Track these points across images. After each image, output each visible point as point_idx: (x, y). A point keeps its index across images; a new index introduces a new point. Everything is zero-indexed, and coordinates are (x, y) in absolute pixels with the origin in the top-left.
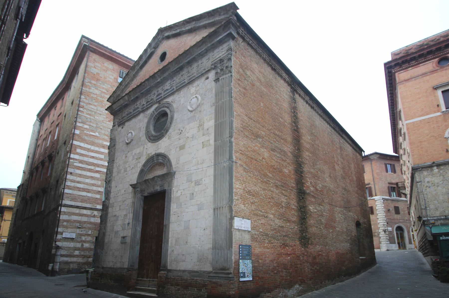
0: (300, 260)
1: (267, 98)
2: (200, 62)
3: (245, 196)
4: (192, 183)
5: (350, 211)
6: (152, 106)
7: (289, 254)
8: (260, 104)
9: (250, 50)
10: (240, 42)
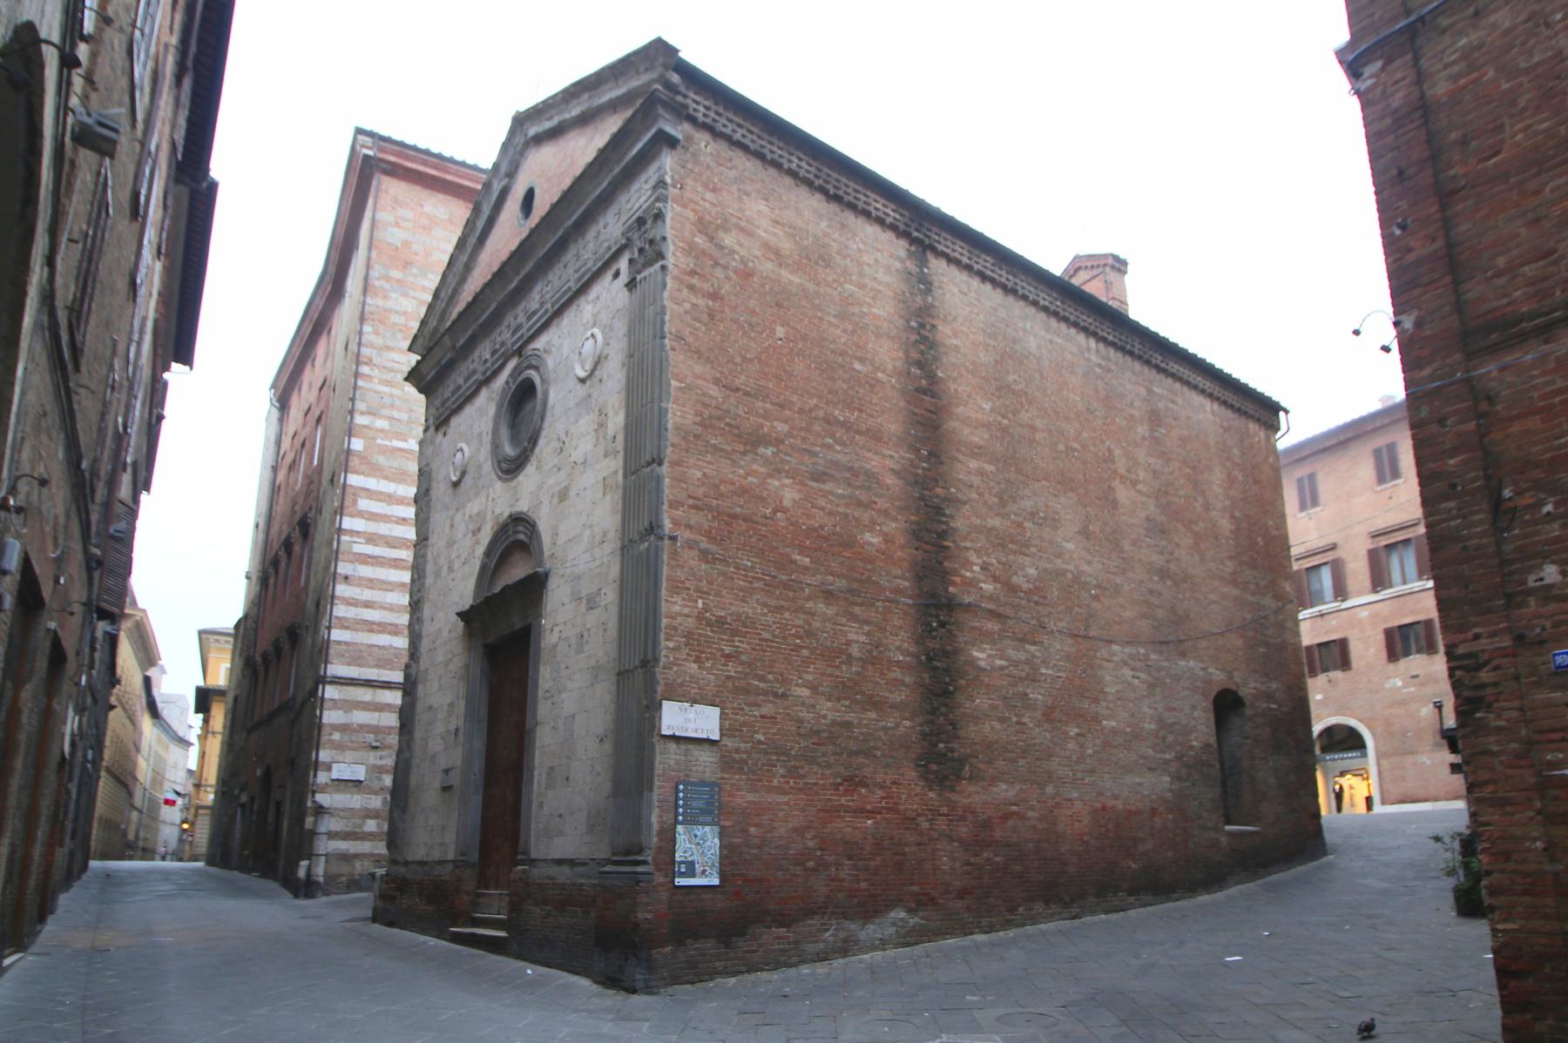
1: (803, 303)
2: (601, 224)
3: (705, 636)
5: (1183, 655)
8: (773, 331)
9: (739, 158)
10: (699, 144)
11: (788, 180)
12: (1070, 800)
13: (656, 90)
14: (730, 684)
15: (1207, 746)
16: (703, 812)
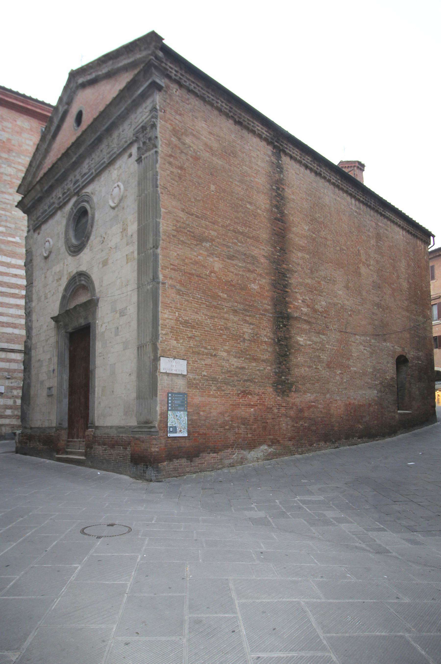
0: (272, 413)
1: (223, 174)
2: (121, 129)
3: (179, 328)
4: (116, 313)
5: (385, 341)
6: (69, 200)
7: (252, 405)
8: (209, 187)
10: (172, 90)
11: (216, 112)
12: (336, 400)
13: (150, 60)
14: (191, 350)
15: (392, 378)
16: (180, 405)
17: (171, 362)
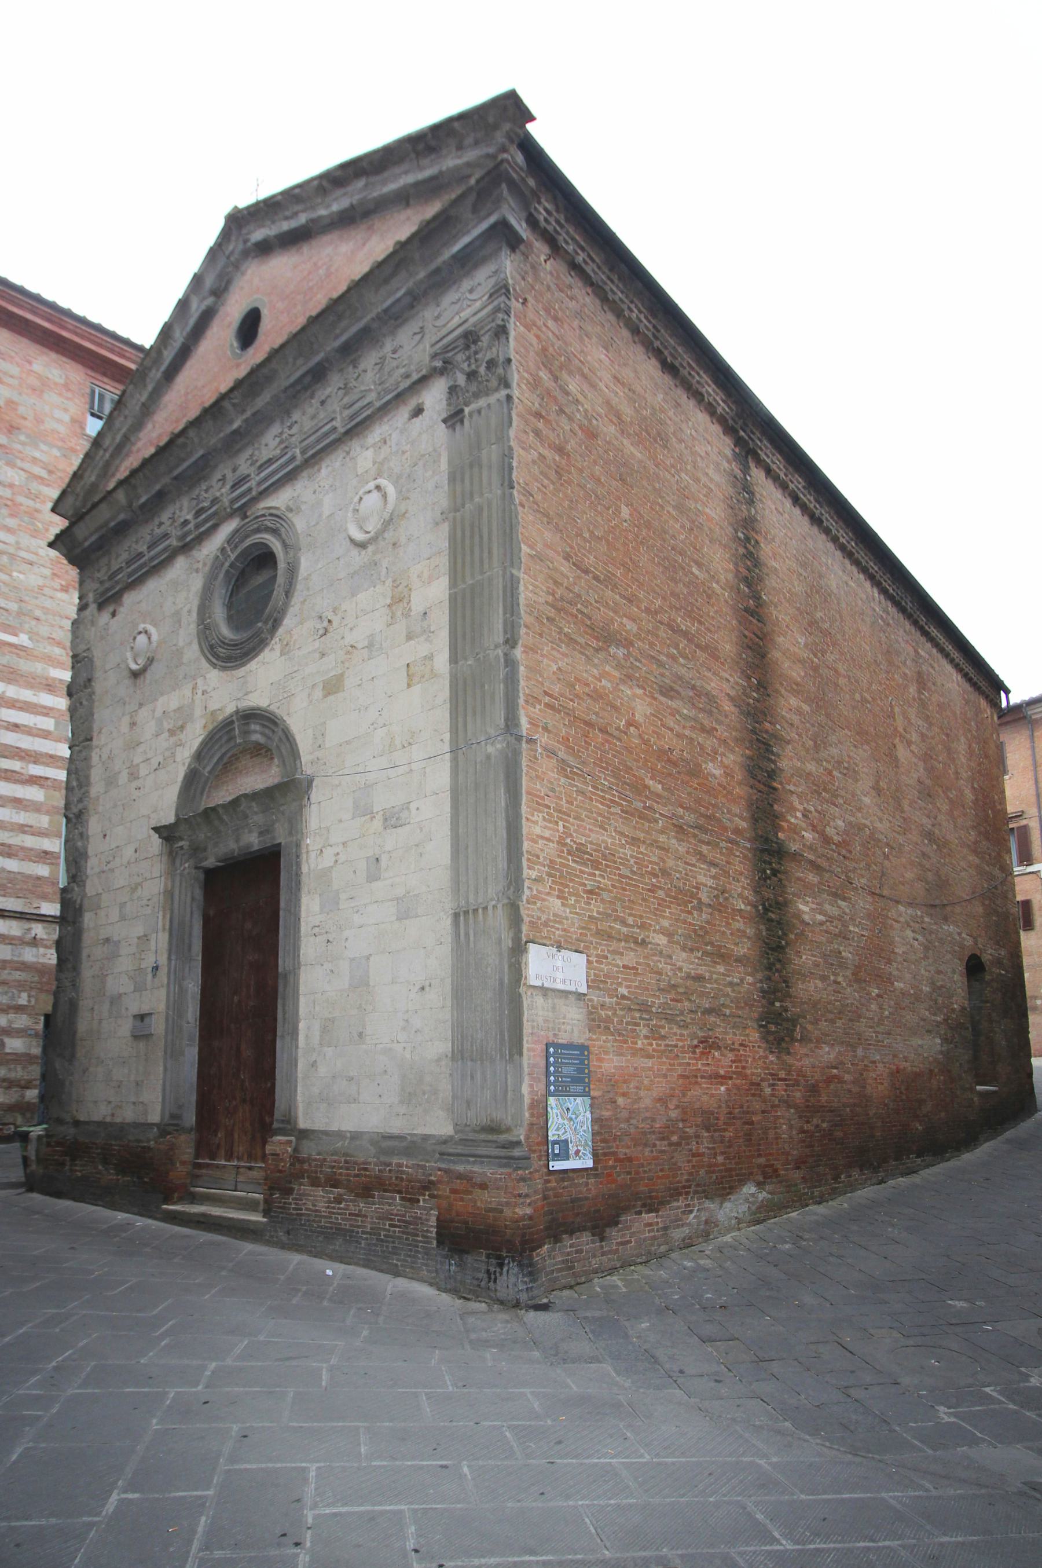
0: (760, 1096)
1: (645, 483)
2: (388, 347)
3: (567, 866)
5: (945, 919)
6: (215, 527)
7: (722, 1077)
8: (618, 510)
10: (538, 257)
11: (625, 333)
12: (874, 1062)
17: (553, 956)
